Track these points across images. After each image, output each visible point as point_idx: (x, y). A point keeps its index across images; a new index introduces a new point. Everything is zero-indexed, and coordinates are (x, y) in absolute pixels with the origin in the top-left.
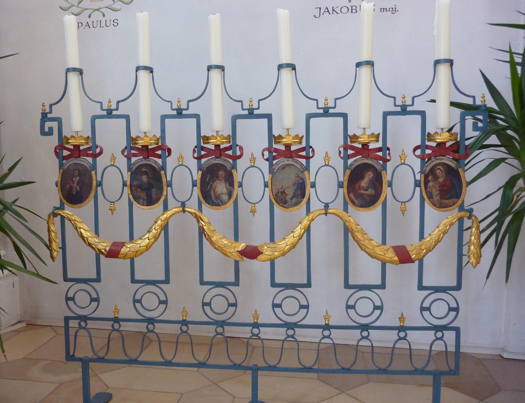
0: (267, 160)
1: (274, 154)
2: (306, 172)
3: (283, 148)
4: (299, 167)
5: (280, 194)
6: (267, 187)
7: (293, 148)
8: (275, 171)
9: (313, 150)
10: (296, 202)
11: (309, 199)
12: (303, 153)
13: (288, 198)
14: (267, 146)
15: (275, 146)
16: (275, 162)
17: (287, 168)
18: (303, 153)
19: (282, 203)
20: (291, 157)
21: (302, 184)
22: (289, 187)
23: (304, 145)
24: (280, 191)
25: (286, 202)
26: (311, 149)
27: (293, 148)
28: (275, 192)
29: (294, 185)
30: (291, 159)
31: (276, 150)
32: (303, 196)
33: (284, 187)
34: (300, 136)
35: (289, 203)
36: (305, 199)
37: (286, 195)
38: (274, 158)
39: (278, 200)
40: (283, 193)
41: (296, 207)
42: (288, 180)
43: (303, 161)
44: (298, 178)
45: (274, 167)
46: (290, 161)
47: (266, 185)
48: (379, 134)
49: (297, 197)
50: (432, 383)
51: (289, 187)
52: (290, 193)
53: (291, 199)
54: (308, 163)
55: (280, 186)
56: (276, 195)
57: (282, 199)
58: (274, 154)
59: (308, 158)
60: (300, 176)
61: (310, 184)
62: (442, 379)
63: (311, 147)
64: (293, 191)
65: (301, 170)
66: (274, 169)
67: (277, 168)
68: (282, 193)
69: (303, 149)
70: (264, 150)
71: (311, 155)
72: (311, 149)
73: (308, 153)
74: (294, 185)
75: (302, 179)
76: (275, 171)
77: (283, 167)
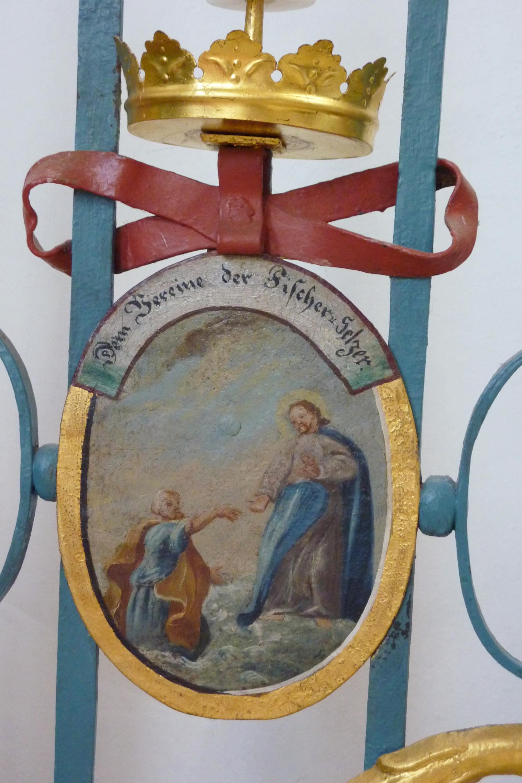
0: (61, 258)
1: (126, 215)
2: (386, 396)
3: (202, 165)
4: (328, 340)
5: (149, 567)
6: (52, 497)
7: (289, 174)
8: (122, 360)
9: (465, 203)
10: (280, 649)
11: (400, 630)
12: (377, 226)
13: (220, 605)
14: (63, 139)
15: (135, 145)
16: (124, 282)
17: (221, 347)
18: (377, 226)
19: (162, 641)
20: (266, 249)
21: (346, 489)
22: (232, 515)
23: (384, 147)
24: (153, 538)
25: (196, 638)
26: (444, 196)
27: (289, 174)
28: (108, 542)
29: (278, 499)
30: (260, 269)
31: (138, 180)
32: (351, 599)
33: (194, 504)
34: (353, 60)
35: (226, 645)
36: (365, 632)
37: (204, 575)
38: (123, 250)
39: (134, 620)
40: (178, 554)
41: (276, 690)
42: (222, 459)
43: (372, 293)
44: (317, 444)
45: (110, 329)
46: (254, 287)
47: (37, 486)
48: (376, 71)
49: (299, 604)
50: (369, 390)
51: (232, 515)
52: (238, 558)
53: (246, 619)
54: (411, 316)
55: (159, 499)
56: (119, 573)
57: (166, 609)
58: (126, 215)
59: (412, 268)
60: (337, 422)
61: (412, 503)
62: (378, 401)
63: (446, 174)
64: (267, 554)
65: (349, 368)
66: (111, 347)
67: (136, 339)
68: (166, 555)
69: (376, 188)
70: (37, 175)
71: (442, 242)
72: (444, 196)
73: (415, 223)
74: (278, 499)
75: (355, 451)
76: (122, 360)
77: (195, 338)
